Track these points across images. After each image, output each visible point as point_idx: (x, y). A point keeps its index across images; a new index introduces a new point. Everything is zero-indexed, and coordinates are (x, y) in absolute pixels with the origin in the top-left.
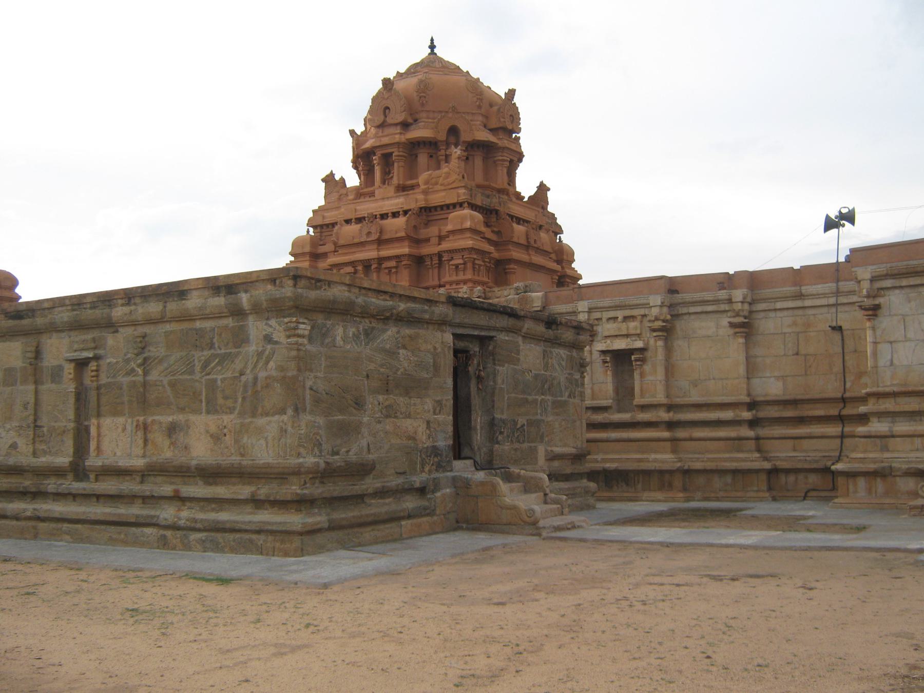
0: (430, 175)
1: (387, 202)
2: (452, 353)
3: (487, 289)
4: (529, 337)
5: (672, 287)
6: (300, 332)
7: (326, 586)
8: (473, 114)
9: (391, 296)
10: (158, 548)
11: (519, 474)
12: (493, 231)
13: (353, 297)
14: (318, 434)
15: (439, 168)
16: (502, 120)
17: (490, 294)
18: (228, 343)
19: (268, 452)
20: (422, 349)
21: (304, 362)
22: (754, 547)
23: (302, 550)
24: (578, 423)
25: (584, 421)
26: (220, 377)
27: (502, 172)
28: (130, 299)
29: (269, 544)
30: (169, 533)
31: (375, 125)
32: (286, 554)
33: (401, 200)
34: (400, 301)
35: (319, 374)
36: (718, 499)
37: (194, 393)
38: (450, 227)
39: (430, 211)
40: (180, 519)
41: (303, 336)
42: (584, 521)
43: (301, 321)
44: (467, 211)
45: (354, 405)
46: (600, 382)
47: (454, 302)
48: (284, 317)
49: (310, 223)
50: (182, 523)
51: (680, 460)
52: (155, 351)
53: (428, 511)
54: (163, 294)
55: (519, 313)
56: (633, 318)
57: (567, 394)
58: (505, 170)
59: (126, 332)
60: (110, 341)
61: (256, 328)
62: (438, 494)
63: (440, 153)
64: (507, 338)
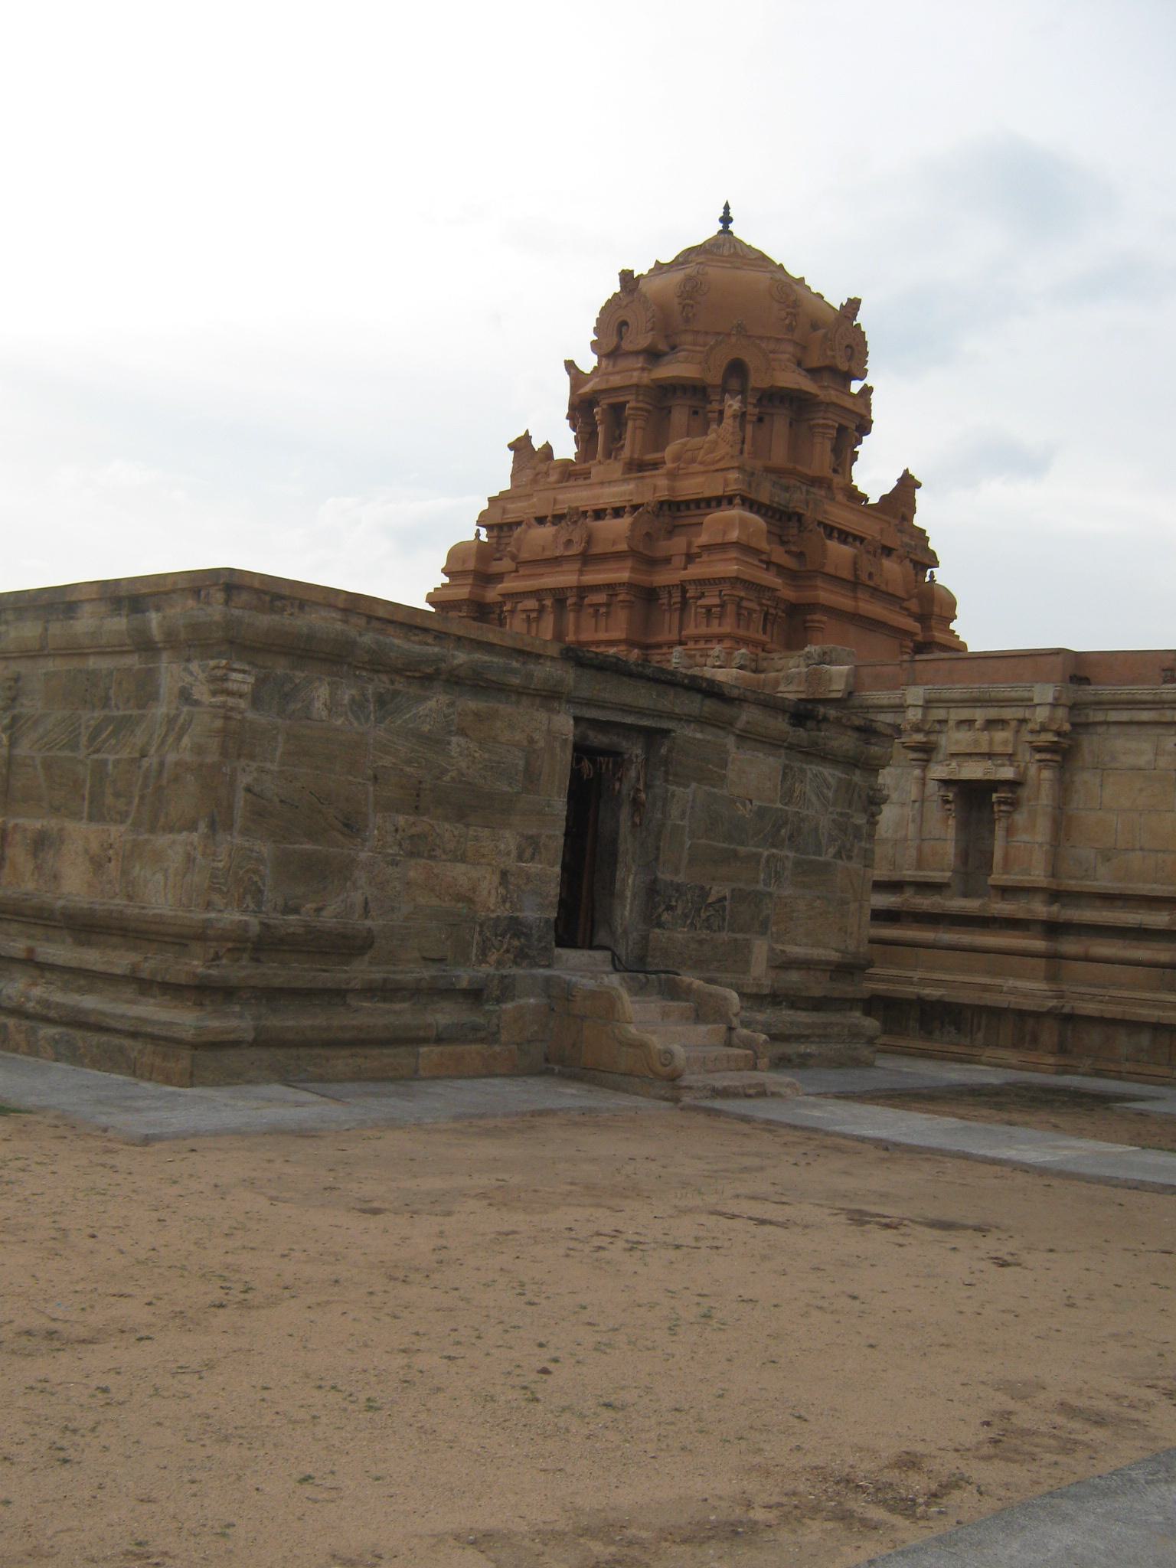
0: (685, 445)
3: (763, 655)
5: (1077, 670)
6: (230, 686)
8: (778, 340)
9: (436, 637)
13: (353, 633)
14: (256, 872)
16: (829, 353)
17: (765, 664)
18: (128, 700)
21: (236, 740)
22: (1042, 1171)
23: (192, 1075)
24: (853, 906)
26: (112, 758)
32: (168, 1081)
35: (268, 765)
36: (1119, 1076)
38: (704, 539)
40: (28, 999)
42: (788, 1085)
43: (236, 666)
48: (212, 658)
51: (1060, 995)
53: (482, 1034)
55: (726, 691)
57: (832, 851)
58: (828, 446)
61: (170, 673)
62: (509, 1006)
63: (709, 407)
64: (699, 736)
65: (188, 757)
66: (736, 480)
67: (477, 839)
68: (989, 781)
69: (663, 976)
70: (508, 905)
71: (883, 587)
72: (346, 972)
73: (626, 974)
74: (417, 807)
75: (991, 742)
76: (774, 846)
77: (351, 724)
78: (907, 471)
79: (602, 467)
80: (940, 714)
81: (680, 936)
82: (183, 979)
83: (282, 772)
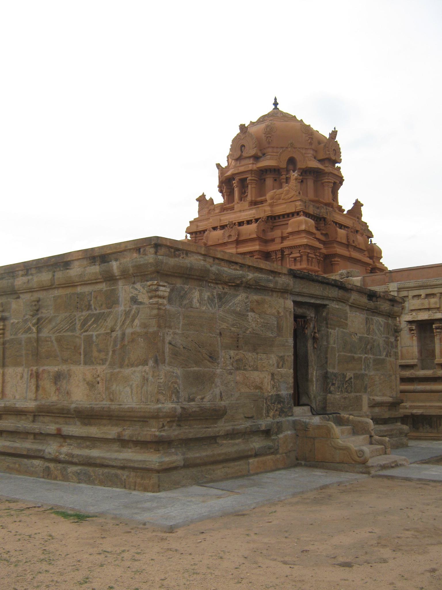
0: (275, 193)
1: (243, 214)
2: (292, 317)
4: (354, 306)
6: (160, 293)
7: (171, 529)
8: (306, 149)
9: (241, 267)
10: (43, 477)
11: (348, 419)
12: (322, 234)
13: (208, 266)
14: (176, 383)
15: (281, 187)
16: (328, 153)
18: (102, 305)
19: (132, 397)
20: (268, 313)
21: (163, 320)
23: (159, 486)
25: (398, 376)
26: (95, 333)
27: (328, 191)
28: (27, 270)
29: (131, 479)
30: (52, 465)
31: (234, 158)
32: (146, 490)
33: (254, 211)
34: (248, 271)
35: (177, 331)
37: (75, 347)
38: (290, 230)
39: (275, 219)
40: (61, 454)
41: (164, 298)
42: (405, 460)
43: (161, 284)
44: (302, 218)
45: (208, 358)
46: (409, 345)
47: (294, 274)
48: (147, 281)
49: (188, 232)
50: (62, 457)
52: (45, 313)
53: (272, 451)
54: (52, 265)
56: (433, 295)
57: (385, 354)
58: (330, 190)
59: (26, 297)
60: (14, 305)
61: (124, 291)
62: (281, 436)
63: (282, 177)
64: (337, 307)
65: (138, 330)
66: (300, 205)
67: (261, 359)
68: (431, 320)
69: (334, 415)
70: (275, 389)
71: (358, 246)
72: (216, 427)
73: (321, 416)
74: (238, 347)
75: (429, 304)
76: (366, 353)
77: (209, 309)
78: (357, 200)
79: (239, 205)
80: (404, 294)
81: (338, 396)
82: (148, 439)
83: (183, 334)
